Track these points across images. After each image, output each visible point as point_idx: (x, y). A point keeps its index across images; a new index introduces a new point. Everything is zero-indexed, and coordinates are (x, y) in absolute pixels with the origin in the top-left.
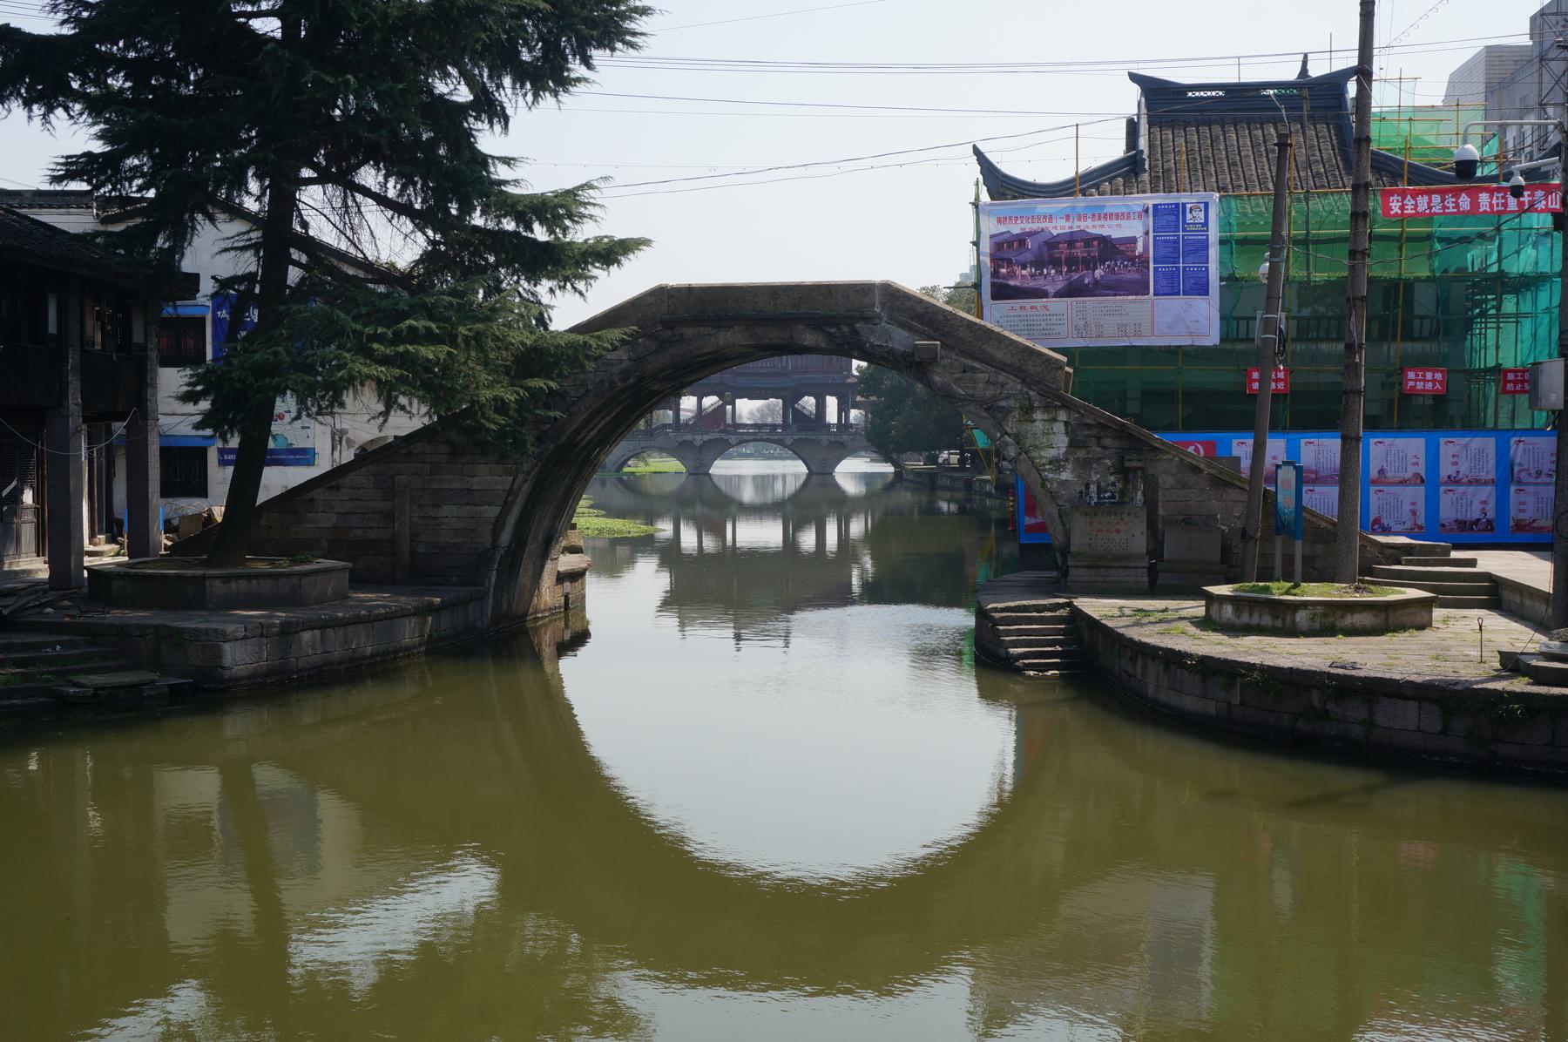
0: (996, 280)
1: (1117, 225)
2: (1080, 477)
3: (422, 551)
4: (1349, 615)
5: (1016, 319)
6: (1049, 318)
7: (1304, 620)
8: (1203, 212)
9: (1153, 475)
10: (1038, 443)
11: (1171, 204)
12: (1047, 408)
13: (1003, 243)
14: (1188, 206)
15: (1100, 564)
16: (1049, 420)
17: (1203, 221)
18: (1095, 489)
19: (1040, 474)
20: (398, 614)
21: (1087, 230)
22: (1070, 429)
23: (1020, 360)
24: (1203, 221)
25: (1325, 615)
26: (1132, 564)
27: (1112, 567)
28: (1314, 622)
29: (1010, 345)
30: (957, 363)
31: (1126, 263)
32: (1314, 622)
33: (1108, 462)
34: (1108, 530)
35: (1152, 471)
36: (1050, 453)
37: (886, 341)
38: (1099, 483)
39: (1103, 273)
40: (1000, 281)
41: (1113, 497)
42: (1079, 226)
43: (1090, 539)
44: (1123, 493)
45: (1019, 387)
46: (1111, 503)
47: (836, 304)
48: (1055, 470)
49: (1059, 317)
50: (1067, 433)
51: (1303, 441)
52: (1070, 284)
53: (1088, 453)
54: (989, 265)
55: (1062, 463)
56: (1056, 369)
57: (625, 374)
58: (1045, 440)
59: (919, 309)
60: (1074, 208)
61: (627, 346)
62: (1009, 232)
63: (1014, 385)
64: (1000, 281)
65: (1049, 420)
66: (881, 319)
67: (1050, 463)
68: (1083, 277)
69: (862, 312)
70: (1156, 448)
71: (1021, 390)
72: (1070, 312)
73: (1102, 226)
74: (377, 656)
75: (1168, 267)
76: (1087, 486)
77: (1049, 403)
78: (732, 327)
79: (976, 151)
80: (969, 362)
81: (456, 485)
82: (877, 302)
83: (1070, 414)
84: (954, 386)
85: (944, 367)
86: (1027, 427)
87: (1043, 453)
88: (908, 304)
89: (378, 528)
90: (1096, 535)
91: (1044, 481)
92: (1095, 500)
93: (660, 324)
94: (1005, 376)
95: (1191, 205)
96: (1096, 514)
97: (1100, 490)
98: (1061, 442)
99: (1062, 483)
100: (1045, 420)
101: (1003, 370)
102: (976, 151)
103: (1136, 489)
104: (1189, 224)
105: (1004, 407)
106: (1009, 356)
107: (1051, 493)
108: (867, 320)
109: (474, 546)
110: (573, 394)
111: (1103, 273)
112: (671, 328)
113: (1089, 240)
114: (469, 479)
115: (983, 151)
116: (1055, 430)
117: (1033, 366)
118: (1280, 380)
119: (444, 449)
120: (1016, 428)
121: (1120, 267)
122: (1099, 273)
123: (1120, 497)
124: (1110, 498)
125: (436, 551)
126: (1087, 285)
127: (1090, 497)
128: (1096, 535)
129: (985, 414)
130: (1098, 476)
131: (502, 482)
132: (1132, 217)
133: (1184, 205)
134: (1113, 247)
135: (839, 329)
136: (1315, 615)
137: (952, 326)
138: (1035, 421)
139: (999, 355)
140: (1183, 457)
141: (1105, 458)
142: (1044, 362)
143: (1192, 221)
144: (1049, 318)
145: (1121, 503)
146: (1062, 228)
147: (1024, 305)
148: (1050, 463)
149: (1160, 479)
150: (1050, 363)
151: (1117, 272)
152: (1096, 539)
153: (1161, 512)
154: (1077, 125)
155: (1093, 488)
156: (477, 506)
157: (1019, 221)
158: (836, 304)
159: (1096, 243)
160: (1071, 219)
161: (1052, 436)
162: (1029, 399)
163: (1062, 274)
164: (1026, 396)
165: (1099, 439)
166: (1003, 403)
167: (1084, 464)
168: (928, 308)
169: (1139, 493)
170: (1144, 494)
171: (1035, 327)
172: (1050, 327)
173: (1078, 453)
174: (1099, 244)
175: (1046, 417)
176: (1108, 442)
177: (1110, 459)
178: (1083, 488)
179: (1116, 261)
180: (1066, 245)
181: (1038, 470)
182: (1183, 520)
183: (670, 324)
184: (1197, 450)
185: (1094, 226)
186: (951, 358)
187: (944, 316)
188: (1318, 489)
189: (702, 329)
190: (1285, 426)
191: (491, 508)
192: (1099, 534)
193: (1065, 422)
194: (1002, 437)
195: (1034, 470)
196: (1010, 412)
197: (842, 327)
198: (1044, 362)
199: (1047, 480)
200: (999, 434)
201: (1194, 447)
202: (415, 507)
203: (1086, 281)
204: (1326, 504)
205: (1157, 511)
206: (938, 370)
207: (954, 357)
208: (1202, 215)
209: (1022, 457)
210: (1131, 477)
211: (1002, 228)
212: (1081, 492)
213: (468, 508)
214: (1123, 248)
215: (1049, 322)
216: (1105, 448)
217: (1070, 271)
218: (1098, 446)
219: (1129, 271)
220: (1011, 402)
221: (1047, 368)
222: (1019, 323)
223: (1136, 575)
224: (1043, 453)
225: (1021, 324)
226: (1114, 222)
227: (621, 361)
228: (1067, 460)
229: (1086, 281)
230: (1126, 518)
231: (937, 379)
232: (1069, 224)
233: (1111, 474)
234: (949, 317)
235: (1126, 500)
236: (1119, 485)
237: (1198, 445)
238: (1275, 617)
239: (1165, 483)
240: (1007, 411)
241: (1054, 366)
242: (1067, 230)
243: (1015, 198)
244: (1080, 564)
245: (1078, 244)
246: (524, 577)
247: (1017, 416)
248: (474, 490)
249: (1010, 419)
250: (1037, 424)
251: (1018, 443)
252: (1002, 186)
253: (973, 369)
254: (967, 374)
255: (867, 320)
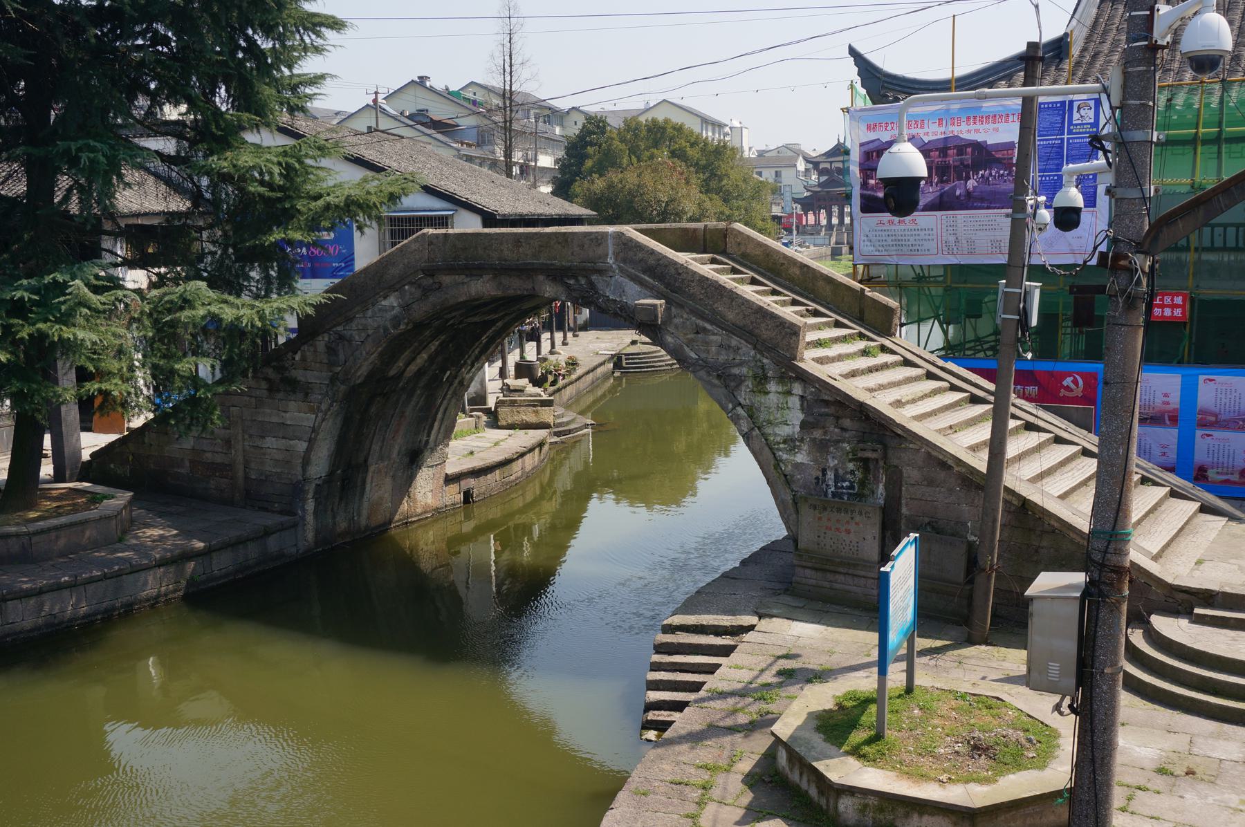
0: (865, 192)
1: (994, 129)
2: (816, 461)
3: (253, 477)
4: (916, 816)
5: (883, 233)
6: (917, 232)
7: (850, 810)
8: (1093, 109)
9: (896, 467)
10: (772, 418)
11: (1056, 103)
12: (782, 379)
13: (872, 152)
14: (1076, 105)
15: (827, 567)
16: (784, 393)
17: (1092, 121)
18: (833, 477)
19: (774, 454)
20: (127, 571)
21: (961, 136)
22: (805, 404)
23: (752, 323)
24: (1092, 121)
25: (881, 810)
26: (862, 573)
27: (840, 573)
28: (864, 816)
29: (743, 304)
30: (688, 323)
31: (1002, 172)
32: (864, 816)
33: (847, 446)
34: (838, 529)
35: (895, 462)
36: (785, 431)
37: (621, 296)
38: (836, 470)
39: (976, 184)
40: (869, 192)
41: (852, 487)
42: (953, 131)
43: (819, 537)
44: (863, 483)
45: (752, 353)
46: (848, 494)
47: (572, 254)
48: (791, 450)
49: (927, 232)
50: (802, 409)
51: (1202, 378)
52: (941, 195)
53: (825, 433)
54: (858, 175)
55: (798, 443)
56: (790, 334)
57: (396, 321)
58: (779, 416)
59: (651, 261)
60: (948, 110)
61: (396, 293)
62: (878, 139)
63: (748, 351)
64: (869, 192)
65: (784, 393)
66: (614, 272)
67: (785, 442)
68: (954, 189)
69: (595, 263)
70: (899, 435)
71: (754, 357)
72: (939, 227)
73: (977, 131)
74: (98, 614)
75: (1049, 176)
76: (824, 471)
77: (783, 373)
78: (481, 276)
79: (853, 52)
80: (701, 323)
81: (275, 419)
82: (610, 252)
83: (805, 387)
84: (686, 348)
85: (676, 327)
86: (761, 398)
87: (777, 430)
88: (640, 255)
89: (222, 453)
90: (825, 533)
91: (778, 461)
92: (833, 489)
93: (420, 272)
94: (738, 341)
95: (1079, 102)
96: (825, 509)
97: (838, 478)
98: (796, 417)
99: (798, 466)
100: (779, 393)
101: (734, 335)
102: (853, 52)
103: (877, 481)
104: (1077, 125)
105: (735, 375)
106: (741, 316)
107: (785, 476)
108: (600, 272)
109: (290, 476)
110: (357, 338)
111: (976, 184)
112: (432, 276)
113: (962, 146)
114: (283, 414)
115: (862, 52)
116: (790, 405)
117: (766, 329)
118: (1177, 306)
119: (264, 385)
120: (749, 399)
121: (995, 176)
122: (971, 183)
123: (859, 488)
124: (848, 488)
125: (263, 478)
126: (958, 197)
127: (827, 485)
128: (825, 533)
129: (716, 382)
130: (836, 462)
131: (308, 420)
132: (1011, 119)
133: (1071, 102)
134: (989, 153)
135: (577, 280)
136: (866, 806)
137: (683, 280)
138: (768, 393)
139: (731, 316)
140: (930, 450)
141: (843, 441)
142: (777, 326)
143: (1079, 122)
144: (917, 232)
145: (860, 496)
146: (935, 133)
147: (882, 219)
148: (785, 442)
149: (904, 471)
150: (784, 327)
151: (991, 183)
152: (824, 538)
153: (904, 510)
154: (954, 16)
155: (830, 475)
156: (291, 440)
157: (889, 128)
158: (572, 254)
159: (969, 150)
160: (944, 122)
161: (787, 412)
162: (763, 368)
163: (932, 185)
164: (759, 364)
165: (838, 418)
166: (736, 371)
167: (821, 447)
168: (659, 260)
169: (881, 486)
170: (886, 488)
171: (904, 243)
172: (918, 243)
173: (814, 433)
174: (973, 151)
175: (780, 389)
176: (847, 423)
177: (849, 442)
178: (820, 474)
179: (991, 170)
180: (937, 153)
181: (771, 449)
182: (929, 523)
183: (430, 272)
184: (1075, 382)
185: (969, 131)
186: (682, 317)
187: (676, 269)
188: (1217, 434)
189: (457, 277)
190: (1183, 357)
191: (301, 442)
192: (827, 531)
193: (802, 397)
194: (734, 408)
195: (767, 449)
196: (742, 381)
197: (580, 278)
198: (777, 326)
199: (781, 461)
200: (730, 406)
201: (1072, 378)
202: (246, 437)
203: (958, 193)
204: (1226, 451)
205: (899, 510)
206: (671, 329)
207: (685, 316)
208: (1091, 113)
209: (754, 433)
210: (872, 467)
211: (872, 136)
212: (817, 478)
213: (284, 441)
214: (999, 155)
215: (917, 238)
216: (843, 429)
217: (941, 181)
218: (835, 427)
219: (1005, 181)
220: (745, 370)
221: (781, 333)
222: (887, 238)
223: (865, 586)
224: (777, 430)
225: (889, 239)
226: (991, 126)
227: (393, 307)
228: (802, 440)
229: (958, 193)
230: (858, 518)
231: (669, 339)
232: (943, 129)
233: (850, 461)
234: (681, 272)
235: (866, 492)
236: (859, 475)
237: (1077, 376)
238: (821, 793)
239: (909, 477)
240: (740, 380)
241: (788, 330)
242: (940, 136)
243: (897, 100)
244: (804, 564)
245: (950, 152)
246: (377, 488)
247: (750, 386)
248: (287, 425)
249: (743, 389)
250: (771, 396)
251: (751, 417)
252: (883, 87)
253: (705, 330)
254: (699, 336)
255: (600, 272)
